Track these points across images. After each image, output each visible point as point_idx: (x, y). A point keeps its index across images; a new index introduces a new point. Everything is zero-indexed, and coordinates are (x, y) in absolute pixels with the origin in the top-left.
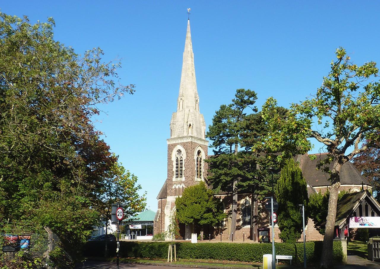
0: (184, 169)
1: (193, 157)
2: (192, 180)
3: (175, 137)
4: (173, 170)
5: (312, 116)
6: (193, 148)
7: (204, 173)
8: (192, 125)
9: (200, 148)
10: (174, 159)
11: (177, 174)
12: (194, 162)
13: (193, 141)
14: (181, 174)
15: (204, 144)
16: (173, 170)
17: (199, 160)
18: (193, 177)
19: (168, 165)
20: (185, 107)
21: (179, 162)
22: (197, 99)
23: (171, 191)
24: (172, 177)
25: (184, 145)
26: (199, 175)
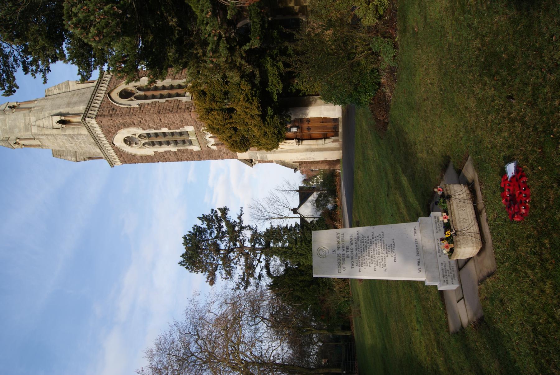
0: (165, 130)
1: (132, 111)
2: (188, 108)
3: (98, 151)
4: (176, 150)
5: (371, 243)
6: (111, 112)
7: (174, 78)
8: (58, 118)
9: (115, 95)
10: (149, 151)
11: (184, 142)
12: (146, 106)
13: (95, 113)
14: (181, 134)
15: (107, 83)
16: (176, 150)
17: (142, 93)
18: (180, 106)
19: (166, 160)
20: (28, 135)
21: (155, 140)
22: (7, 108)
23: (224, 153)
24: (192, 152)
25: (110, 133)
26: (179, 91)
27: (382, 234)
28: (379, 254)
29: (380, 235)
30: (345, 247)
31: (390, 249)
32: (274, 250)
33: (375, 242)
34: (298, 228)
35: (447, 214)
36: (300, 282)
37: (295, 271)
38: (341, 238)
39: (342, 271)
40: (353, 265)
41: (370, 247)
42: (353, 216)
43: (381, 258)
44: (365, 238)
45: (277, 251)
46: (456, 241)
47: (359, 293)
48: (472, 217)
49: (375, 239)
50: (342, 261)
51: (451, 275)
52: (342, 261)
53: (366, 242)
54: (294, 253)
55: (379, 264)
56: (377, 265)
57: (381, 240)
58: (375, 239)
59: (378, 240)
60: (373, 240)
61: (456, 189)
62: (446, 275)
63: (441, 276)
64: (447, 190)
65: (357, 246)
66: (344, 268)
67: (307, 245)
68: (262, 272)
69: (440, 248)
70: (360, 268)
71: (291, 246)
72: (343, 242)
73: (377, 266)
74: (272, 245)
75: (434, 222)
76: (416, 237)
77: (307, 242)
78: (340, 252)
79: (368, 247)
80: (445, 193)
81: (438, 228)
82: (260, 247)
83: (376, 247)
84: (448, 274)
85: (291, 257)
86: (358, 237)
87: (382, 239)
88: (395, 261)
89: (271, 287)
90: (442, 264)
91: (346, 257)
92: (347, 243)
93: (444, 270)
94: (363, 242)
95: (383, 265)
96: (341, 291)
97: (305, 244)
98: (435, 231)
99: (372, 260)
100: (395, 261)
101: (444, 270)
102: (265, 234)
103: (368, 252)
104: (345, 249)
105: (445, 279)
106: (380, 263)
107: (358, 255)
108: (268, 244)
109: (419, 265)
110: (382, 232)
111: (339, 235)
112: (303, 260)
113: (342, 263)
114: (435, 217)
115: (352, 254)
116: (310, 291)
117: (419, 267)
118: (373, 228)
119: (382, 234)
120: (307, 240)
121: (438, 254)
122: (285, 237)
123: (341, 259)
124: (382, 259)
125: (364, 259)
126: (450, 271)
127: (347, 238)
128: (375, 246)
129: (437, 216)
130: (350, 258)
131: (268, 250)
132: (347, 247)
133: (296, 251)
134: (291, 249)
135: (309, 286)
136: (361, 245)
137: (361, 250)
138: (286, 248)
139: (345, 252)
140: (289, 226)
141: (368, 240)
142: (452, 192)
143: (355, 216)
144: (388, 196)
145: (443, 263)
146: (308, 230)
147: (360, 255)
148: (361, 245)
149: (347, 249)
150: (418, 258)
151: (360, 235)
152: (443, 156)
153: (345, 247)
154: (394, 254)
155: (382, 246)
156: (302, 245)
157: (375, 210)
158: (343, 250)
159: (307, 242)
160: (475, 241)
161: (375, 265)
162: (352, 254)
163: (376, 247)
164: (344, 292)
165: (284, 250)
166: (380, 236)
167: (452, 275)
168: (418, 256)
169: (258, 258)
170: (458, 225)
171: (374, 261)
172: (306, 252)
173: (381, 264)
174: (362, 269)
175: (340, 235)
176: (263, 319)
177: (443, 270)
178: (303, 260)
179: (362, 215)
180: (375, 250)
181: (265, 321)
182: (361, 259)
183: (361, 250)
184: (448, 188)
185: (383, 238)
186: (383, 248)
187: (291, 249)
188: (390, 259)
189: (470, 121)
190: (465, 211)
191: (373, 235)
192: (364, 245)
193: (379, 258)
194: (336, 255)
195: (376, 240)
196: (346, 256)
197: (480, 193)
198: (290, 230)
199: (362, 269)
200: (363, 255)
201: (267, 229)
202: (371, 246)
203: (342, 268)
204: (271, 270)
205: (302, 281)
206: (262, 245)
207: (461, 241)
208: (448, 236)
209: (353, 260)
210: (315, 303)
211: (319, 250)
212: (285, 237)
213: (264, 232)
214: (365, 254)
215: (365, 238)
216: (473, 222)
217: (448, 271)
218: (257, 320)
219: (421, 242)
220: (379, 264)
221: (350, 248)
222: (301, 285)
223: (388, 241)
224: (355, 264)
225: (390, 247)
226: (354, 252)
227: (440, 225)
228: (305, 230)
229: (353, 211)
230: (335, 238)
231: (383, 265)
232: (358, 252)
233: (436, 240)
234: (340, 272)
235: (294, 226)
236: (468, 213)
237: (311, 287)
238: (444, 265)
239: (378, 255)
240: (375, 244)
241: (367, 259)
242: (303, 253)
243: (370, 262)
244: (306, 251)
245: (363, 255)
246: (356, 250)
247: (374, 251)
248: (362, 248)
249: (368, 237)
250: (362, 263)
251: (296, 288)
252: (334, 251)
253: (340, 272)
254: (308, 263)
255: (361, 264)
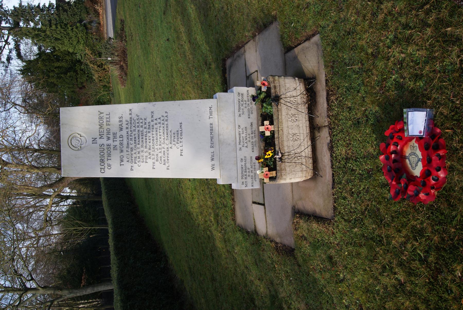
27: (166, 114)
28: (160, 145)
29: (163, 116)
30: (111, 133)
31: (176, 137)
32: (24, 32)
33: (155, 126)
34: (53, 8)
35: (272, 123)
36: (56, 68)
37: (50, 56)
38: (105, 120)
39: (106, 169)
40: (122, 161)
41: (148, 134)
42: (117, 11)
43: (163, 150)
44: (141, 121)
45: (28, 33)
46: (281, 170)
47: (120, 92)
48: (305, 132)
49: (155, 122)
50: (106, 155)
51: (251, 174)
52: (106, 155)
53: (142, 127)
54: (48, 37)
55: (159, 159)
56: (157, 161)
57: (163, 124)
58: (155, 122)
59: (160, 123)
60: (152, 123)
61: (288, 85)
62: (246, 175)
63: (240, 175)
64: (275, 87)
65: (130, 133)
66: (109, 165)
67: (63, 28)
68: (11, 54)
69: (241, 139)
70: (132, 165)
71: (44, 28)
72: (108, 127)
73: (156, 162)
74: (21, 24)
75: (236, 102)
76: (211, 121)
77: (63, 25)
78: (104, 141)
79: (145, 133)
80: (273, 91)
81: (241, 111)
82: (8, 25)
83: (157, 134)
84: (248, 174)
85: (44, 41)
86: (131, 118)
87: (166, 123)
88: (181, 155)
89: (24, 71)
90: (242, 159)
91: (112, 150)
92: (114, 128)
93: (244, 168)
94: (138, 127)
95: (165, 160)
96: (100, 80)
97: (61, 27)
98: (237, 113)
99: (150, 153)
100: (181, 155)
101: (244, 168)
102: (12, 13)
103: (144, 141)
104: (111, 136)
105: (244, 180)
106: (161, 157)
107: (130, 146)
108: (17, 24)
109: (212, 160)
110: (166, 112)
111: (102, 115)
112: (59, 46)
113: (106, 158)
114: (239, 93)
115: (121, 144)
116: (67, 79)
117: (213, 162)
118: (154, 106)
119: (166, 114)
120: (63, 22)
121: (238, 146)
122: (38, 18)
123: (105, 152)
124: (164, 152)
125: (139, 153)
126: (251, 169)
127: (115, 120)
128: (154, 133)
129: (241, 92)
130: (118, 151)
131: (17, 29)
132: (115, 134)
133: (51, 35)
134: (45, 31)
135: (65, 73)
136: (135, 130)
137: (135, 138)
138: (39, 30)
139: (110, 142)
140: (41, 6)
141: (145, 124)
142: (283, 90)
143: (119, 13)
144: (164, 14)
145: (243, 158)
146: (64, 12)
147: (133, 146)
148: (135, 130)
149: (115, 137)
150: (212, 150)
151: (134, 116)
152: (262, 10)
153: (111, 133)
154: (181, 144)
155: (165, 133)
156: (57, 28)
157: (145, 20)
158: (109, 138)
159: (63, 25)
160: (305, 169)
161: (153, 161)
162: (121, 144)
163: (157, 134)
164: (104, 81)
165: (36, 32)
166: (162, 118)
167: (253, 174)
168: (212, 147)
169: (5, 39)
170: (285, 143)
171: (153, 155)
172: (62, 37)
173: (163, 159)
174: (135, 166)
175: (104, 115)
176: (15, 104)
177: (242, 168)
178: (59, 46)
179: (128, 17)
180: (155, 138)
181: (17, 107)
182: (134, 151)
183: (135, 138)
184: (277, 84)
185: (167, 120)
186: (166, 136)
187: (45, 31)
188: (174, 152)
189: (381, 24)
190: (297, 123)
191: (152, 117)
192: (139, 131)
193: (160, 151)
194: (97, 146)
195: (156, 124)
196: (112, 147)
197: (325, 105)
198: (42, 10)
199: (135, 166)
200: (138, 146)
201: (14, 7)
202: (149, 132)
203: (106, 165)
204: (23, 52)
205: (58, 67)
206: (10, 23)
207: (288, 169)
208: (269, 157)
209: (122, 154)
210: (72, 91)
211: (71, 138)
212: (38, 18)
213: (11, 10)
214: (141, 144)
215: (141, 121)
216: (306, 140)
217: (249, 169)
218: (8, 106)
219: (217, 129)
220: (159, 159)
221: (118, 135)
222: (57, 72)
223: (173, 126)
224: (125, 159)
225: (176, 135)
226: (125, 142)
227: (244, 105)
228: (61, 12)
229: (118, 7)
230: (97, 120)
231: (165, 160)
232: (130, 141)
233: (237, 127)
234: (103, 171)
235: (47, 6)
236: (301, 125)
237: (69, 74)
238: (244, 161)
239: (159, 147)
240: (155, 130)
241: (142, 151)
242: (59, 37)
243: (146, 157)
244: (62, 35)
245: (138, 146)
246: (128, 138)
247: (153, 140)
248: (137, 136)
249: (145, 119)
250: (135, 158)
251: (51, 74)
252: (94, 140)
253: (103, 171)
254: (64, 49)
255: (133, 159)
